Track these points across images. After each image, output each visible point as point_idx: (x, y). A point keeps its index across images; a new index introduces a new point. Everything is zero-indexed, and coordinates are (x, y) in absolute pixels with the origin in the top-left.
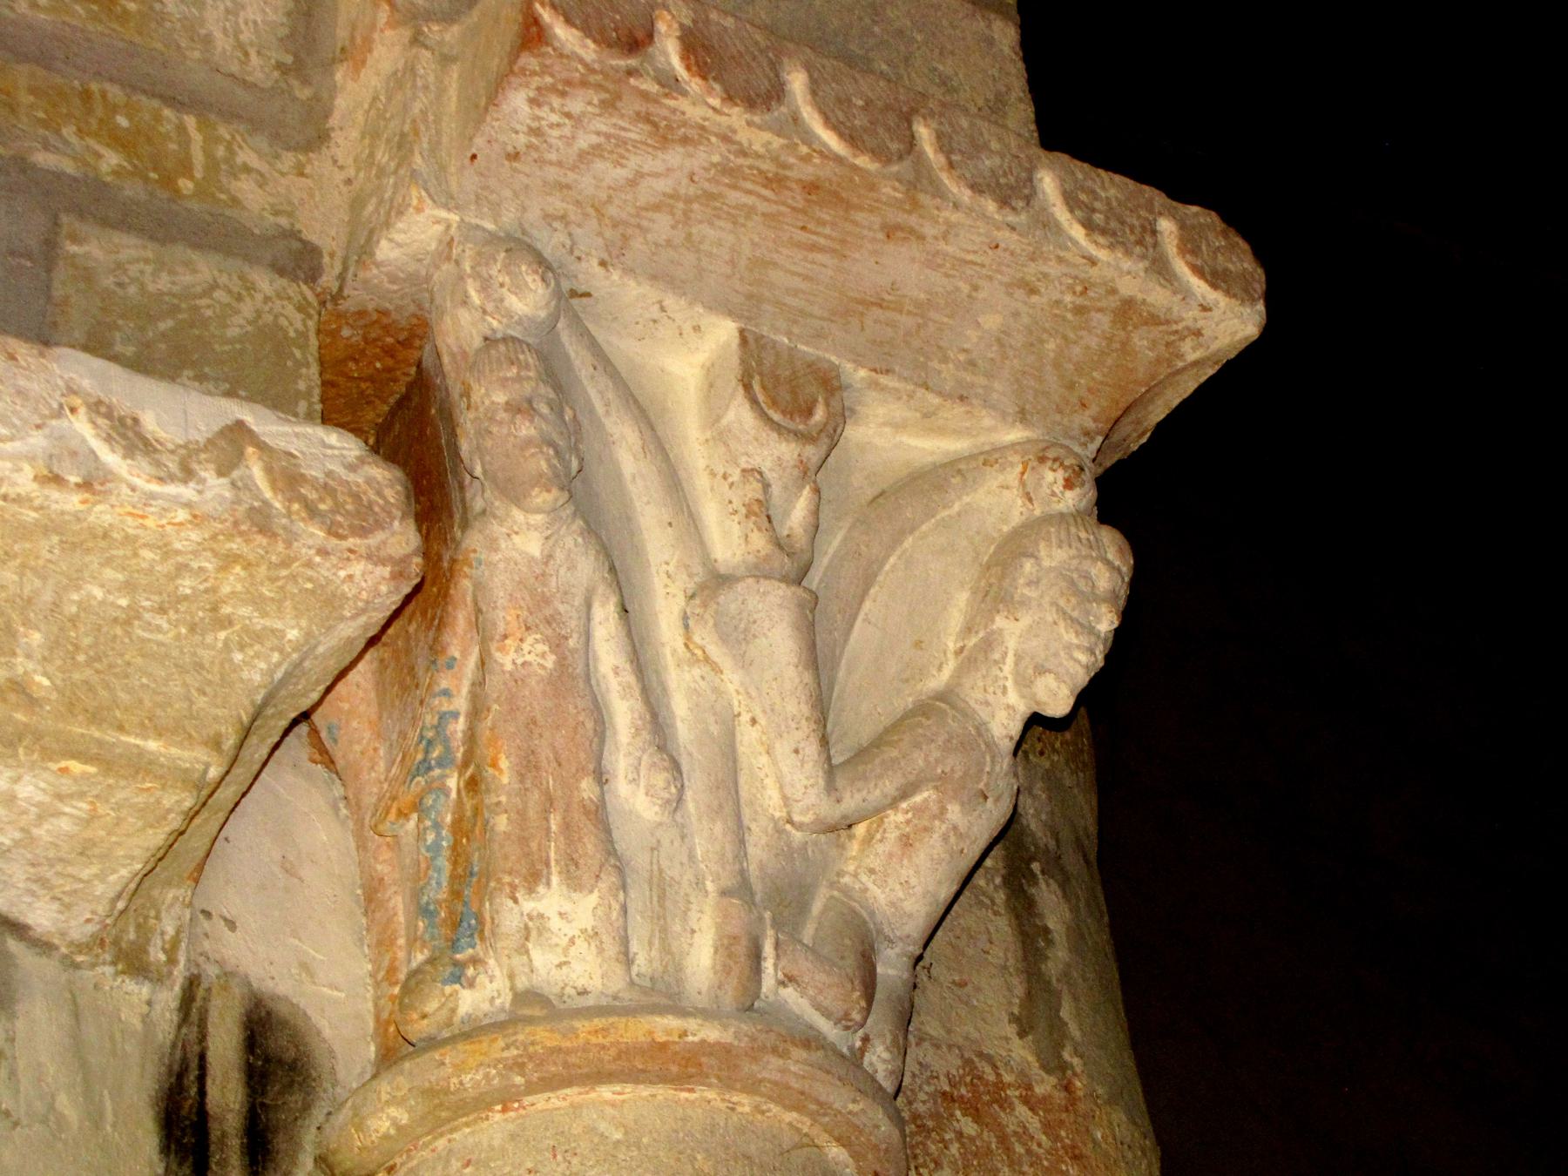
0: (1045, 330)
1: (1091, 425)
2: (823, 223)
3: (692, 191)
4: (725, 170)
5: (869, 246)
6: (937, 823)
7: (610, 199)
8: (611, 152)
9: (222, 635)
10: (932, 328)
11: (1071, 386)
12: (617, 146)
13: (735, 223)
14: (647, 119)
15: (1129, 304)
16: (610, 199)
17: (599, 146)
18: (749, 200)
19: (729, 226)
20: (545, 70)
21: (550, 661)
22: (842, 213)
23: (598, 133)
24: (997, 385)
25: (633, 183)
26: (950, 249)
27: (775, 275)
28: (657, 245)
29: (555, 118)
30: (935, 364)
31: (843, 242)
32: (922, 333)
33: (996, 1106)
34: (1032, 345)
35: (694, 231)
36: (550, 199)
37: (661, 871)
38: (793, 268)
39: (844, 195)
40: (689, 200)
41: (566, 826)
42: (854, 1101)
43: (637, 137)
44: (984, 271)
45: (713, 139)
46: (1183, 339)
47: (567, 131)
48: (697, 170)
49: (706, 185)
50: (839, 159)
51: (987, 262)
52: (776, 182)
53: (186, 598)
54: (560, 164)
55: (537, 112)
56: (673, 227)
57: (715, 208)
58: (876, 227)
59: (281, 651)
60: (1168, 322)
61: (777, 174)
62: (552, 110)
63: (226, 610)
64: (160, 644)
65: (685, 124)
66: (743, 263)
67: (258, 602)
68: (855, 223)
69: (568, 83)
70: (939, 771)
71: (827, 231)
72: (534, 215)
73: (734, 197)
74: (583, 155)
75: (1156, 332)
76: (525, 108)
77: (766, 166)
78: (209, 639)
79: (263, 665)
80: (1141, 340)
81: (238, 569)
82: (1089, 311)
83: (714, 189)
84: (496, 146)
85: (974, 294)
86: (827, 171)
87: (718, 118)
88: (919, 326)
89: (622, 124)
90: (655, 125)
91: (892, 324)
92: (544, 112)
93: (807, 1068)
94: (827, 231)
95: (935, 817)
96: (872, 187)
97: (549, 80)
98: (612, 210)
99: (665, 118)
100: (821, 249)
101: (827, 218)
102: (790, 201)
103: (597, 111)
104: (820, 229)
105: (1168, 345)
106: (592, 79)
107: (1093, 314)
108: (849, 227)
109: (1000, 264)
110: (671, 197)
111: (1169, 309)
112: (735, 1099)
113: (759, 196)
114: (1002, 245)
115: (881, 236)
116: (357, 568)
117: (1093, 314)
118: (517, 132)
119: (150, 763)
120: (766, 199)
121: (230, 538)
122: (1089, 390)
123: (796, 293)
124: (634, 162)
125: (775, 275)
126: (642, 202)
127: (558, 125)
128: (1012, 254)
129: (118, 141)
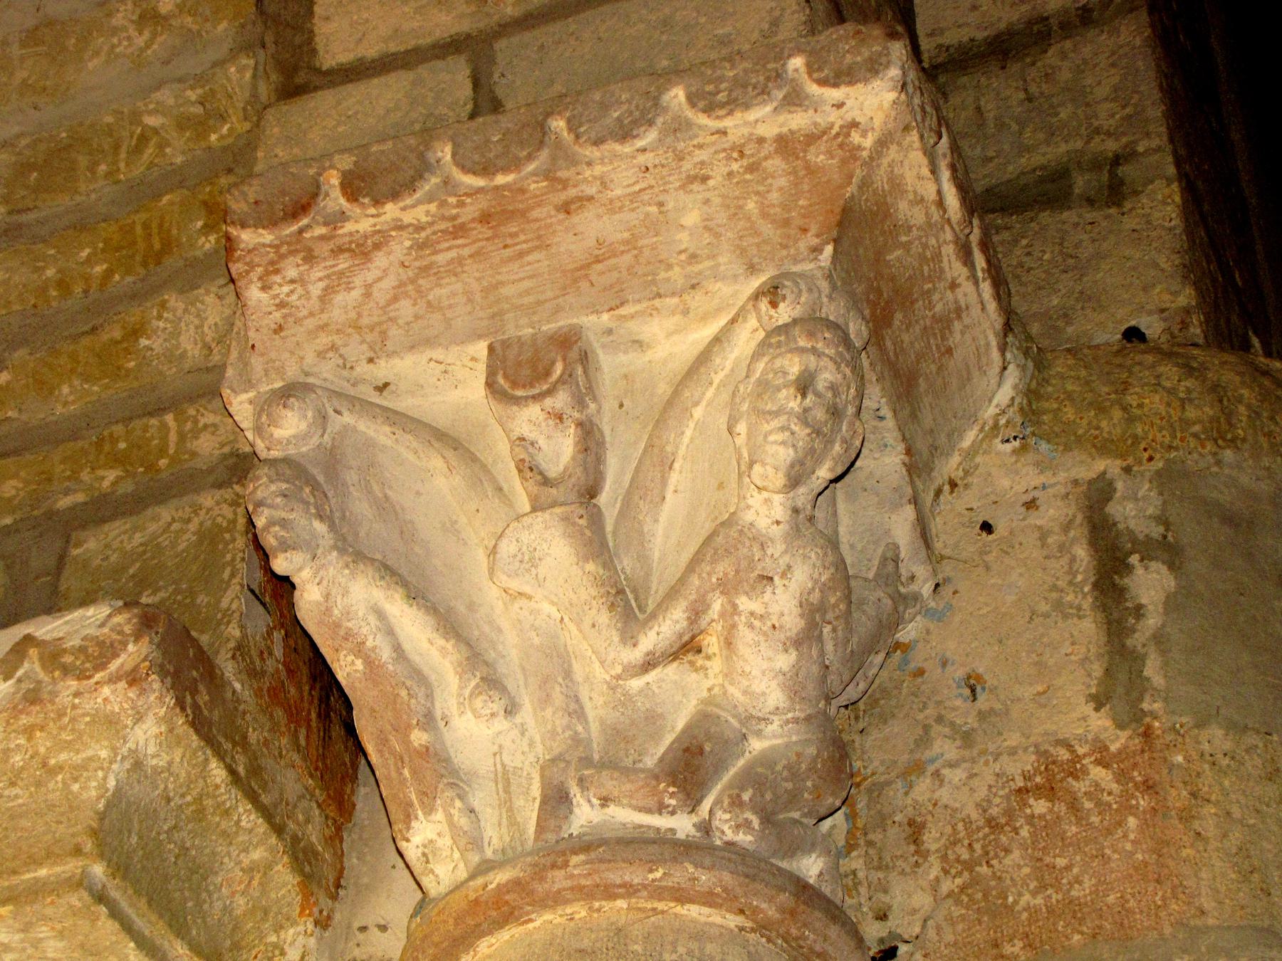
0: (737, 198)
1: (816, 241)
3: (410, 274)
6: (736, 618)
7: (359, 315)
9: (60, 777)
10: (647, 252)
11: (786, 223)
12: (339, 279)
13: (456, 275)
14: (340, 250)
16: (359, 315)
17: (325, 289)
19: (453, 279)
20: (252, 266)
21: (359, 665)
23: (320, 279)
24: (721, 260)
25: (368, 295)
27: (507, 291)
28: (408, 324)
29: (286, 289)
30: (663, 275)
31: (539, 237)
32: (641, 260)
33: (1070, 779)
34: (736, 214)
35: (430, 297)
36: (318, 341)
37: (504, 766)
38: (516, 277)
40: (413, 281)
41: (414, 772)
42: (651, 871)
43: (346, 265)
44: (656, 190)
45: (393, 233)
46: (848, 135)
47: (300, 291)
48: (402, 258)
49: (417, 264)
50: (480, 190)
51: (653, 182)
52: (459, 231)
53: (22, 768)
54: (311, 314)
55: (272, 292)
56: (414, 305)
57: (435, 274)
58: (553, 213)
59: (102, 769)
60: (824, 133)
62: (281, 285)
63: (53, 762)
64: (20, 806)
65: (366, 237)
66: (478, 297)
67: (67, 746)
68: (537, 220)
69: (272, 263)
70: (714, 580)
71: (522, 237)
72: (310, 358)
73: (441, 258)
74: (322, 299)
75: (823, 145)
76: (264, 296)
77: (443, 225)
78: (51, 785)
79: (94, 784)
80: (817, 156)
81: (38, 734)
82: (760, 164)
84: (265, 331)
86: (483, 203)
87: (382, 219)
90: (349, 250)
91: (616, 268)
92: (276, 290)
94: (522, 237)
95: (733, 614)
96: (522, 191)
97: (260, 270)
98: (365, 321)
99: (350, 242)
100: (529, 252)
103: (306, 267)
104: (517, 240)
105: (841, 146)
106: (284, 249)
107: (764, 164)
110: (399, 287)
111: (815, 124)
112: (569, 911)
113: (458, 247)
114: (649, 165)
115: (562, 216)
116: (106, 691)
117: (764, 164)
119: (44, 884)
120: (465, 245)
121: (16, 717)
122: (804, 216)
123: (527, 292)
124: (358, 281)
125: (507, 291)
126: (382, 302)
127: (292, 292)
128: (663, 166)
129: (118, 460)
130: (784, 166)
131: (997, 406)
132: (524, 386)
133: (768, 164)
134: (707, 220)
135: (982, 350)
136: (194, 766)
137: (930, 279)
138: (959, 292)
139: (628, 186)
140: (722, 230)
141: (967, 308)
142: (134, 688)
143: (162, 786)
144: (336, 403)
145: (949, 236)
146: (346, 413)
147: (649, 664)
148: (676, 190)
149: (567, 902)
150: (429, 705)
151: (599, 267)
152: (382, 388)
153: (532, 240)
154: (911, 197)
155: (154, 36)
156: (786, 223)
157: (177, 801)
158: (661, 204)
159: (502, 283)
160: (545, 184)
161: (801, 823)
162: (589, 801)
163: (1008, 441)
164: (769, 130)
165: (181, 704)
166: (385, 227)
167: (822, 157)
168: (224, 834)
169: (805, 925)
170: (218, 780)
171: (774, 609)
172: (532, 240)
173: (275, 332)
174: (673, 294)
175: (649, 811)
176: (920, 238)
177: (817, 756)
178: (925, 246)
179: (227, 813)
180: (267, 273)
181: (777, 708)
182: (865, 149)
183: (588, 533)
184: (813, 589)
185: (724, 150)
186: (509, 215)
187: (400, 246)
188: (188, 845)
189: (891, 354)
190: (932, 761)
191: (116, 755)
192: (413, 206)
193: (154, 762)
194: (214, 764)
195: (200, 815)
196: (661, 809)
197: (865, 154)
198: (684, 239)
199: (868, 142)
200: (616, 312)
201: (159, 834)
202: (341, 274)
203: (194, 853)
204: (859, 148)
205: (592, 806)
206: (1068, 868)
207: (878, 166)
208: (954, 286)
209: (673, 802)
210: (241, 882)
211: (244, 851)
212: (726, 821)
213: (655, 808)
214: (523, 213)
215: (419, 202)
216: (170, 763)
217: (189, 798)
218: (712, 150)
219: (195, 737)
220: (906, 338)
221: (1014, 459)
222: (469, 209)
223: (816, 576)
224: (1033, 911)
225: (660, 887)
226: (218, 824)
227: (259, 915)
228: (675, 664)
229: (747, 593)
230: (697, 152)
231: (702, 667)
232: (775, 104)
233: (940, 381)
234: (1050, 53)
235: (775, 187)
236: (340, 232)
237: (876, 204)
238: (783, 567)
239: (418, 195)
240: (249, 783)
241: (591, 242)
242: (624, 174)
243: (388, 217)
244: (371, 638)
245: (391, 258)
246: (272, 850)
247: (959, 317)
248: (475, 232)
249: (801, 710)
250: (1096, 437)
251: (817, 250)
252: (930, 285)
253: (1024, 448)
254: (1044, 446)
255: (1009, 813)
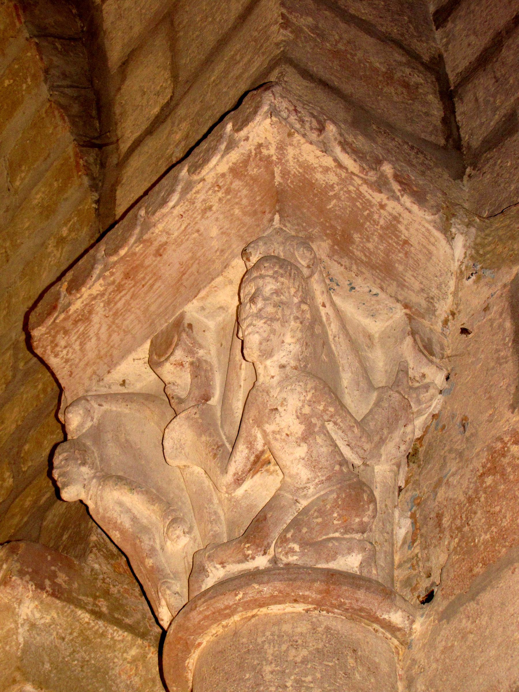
0: (229, 211)
2: (144, 278)
3: (111, 319)
4: (108, 303)
5: (161, 265)
7: (99, 351)
8: (85, 340)
10: (202, 259)
12: (83, 336)
14: (76, 322)
15: (232, 170)
16: (99, 351)
18: (123, 301)
19: (129, 313)
22: (142, 269)
23: (76, 341)
25: (98, 339)
26: (176, 234)
27: (153, 308)
29: (65, 352)
31: (155, 274)
39: (134, 265)
40: (113, 322)
42: (236, 595)
44: (192, 224)
45: (93, 302)
46: (261, 152)
48: (104, 313)
49: (111, 313)
51: (188, 221)
52: (119, 288)
54: (80, 360)
56: (119, 334)
58: (154, 259)
60: (249, 156)
61: (116, 286)
62: (62, 351)
65: (83, 310)
68: (149, 266)
69: (52, 342)
71: (148, 278)
73: (120, 305)
74: (81, 350)
77: (111, 288)
80: (253, 171)
82: (230, 188)
83: (114, 310)
84: (65, 377)
85: (200, 233)
88: (198, 264)
89: (75, 331)
90: (80, 320)
91: (192, 274)
93: (205, 604)
94: (148, 278)
96: (135, 254)
97: (49, 347)
98: (103, 352)
99: (78, 315)
101: (142, 276)
102: (130, 286)
106: (53, 333)
108: (149, 269)
109: (191, 217)
110: (109, 328)
111: (243, 154)
113: (123, 296)
114: (182, 213)
115: (159, 258)
118: (64, 368)
120: (126, 294)
124: (92, 334)
126: (106, 340)
127: (68, 352)
128: (188, 211)
130: (241, 183)
131: (458, 260)
132: (163, 356)
133: (234, 186)
134: (221, 229)
135: (426, 234)
136: (67, 616)
137: (364, 209)
138: (389, 208)
139: (178, 229)
140: (229, 231)
141: (400, 215)
142: (8, 587)
143: (55, 633)
144: (99, 401)
145: (359, 181)
146: (104, 404)
147: (239, 481)
148: (201, 220)
149: (208, 627)
150: (152, 543)
151: (186, 276)
152: (123, 383)
153: (152, 277)
154: (320, 170)
155: (62, 249)
156: (255, 213)
157: (68, 638)
158: (198, 231)
159: (149, 306)
160: (141, 245)
161: (344, 539)
162: (215, 567)
163: (469, 278)
164: (223, 168)
165: (41, 587)
166: (88, 301)
167: (255, 170)
168: (107, 646)
169: (339, 596)
170: (87, 620)
171: (283, 424)
172: (152, 277)
173: (70, 376)
174: (218, 275)
175: (240, 562)
176: (342, 189)
177: (338, 497)
178: (349, 192)
179: (103, 635)
180: (53, 348)
181: (308, 479)
182: (272, 156)
183: (200, 421)
184: (303, 406)
185: (210, 189)
186: (136, 269)
187: (99, 307)
188: (87, 658)
189: (363, 258)
190: (445, 476)
191: (17, 624)
192: (93, 285)
193: (42, 621)
194: (79, 612)
195: (87, 641)
196: (246, 558)
197: (274, 158)
198: (215, 244)
199: (272, 151)
200: (197, 297)
201: (64, 658)
202: (83, 333)
203: (93, 662)
204: (269, 156)
205: (217, 569)
206: (500, 511)
207: (287, 161)
208: (382, 206)
209: (250, 552)
210: (131, 670)
211: (124, 652)
212: (281, 552)
213: (244, 559)
214: (141, 265)
215: (95, 281)
216: (53, 618)
217: (75, 634)
218: (204, 192)
219: (58, 601)
220: (370, 245)
221: (476, 287)
222: (118, 274)
223: (302, 398)
224: (485, 543)
225: (246, 602)
226: (101, 643)
227: (150, 684)
228: (259, 475)
229: (267, 423)
230: (198, 196)
231: (274, 471)
232: (222, 153)
233: (411, 261)
234: (503, 50)
235: (243, 196)
236: (70, 313)
237: (300, 181)
238: (281, 400)
239: (93, 279)
240: (113, 617)
241: (177, 266)
242: (173, 223)
243: (85, 296)
244: (118, 518)
245: (99, 314)
246: (141, 647)
247: (399, 222)
248: (127, 285)
249: (322, 475)
250: (511, 256)
251: (272, 220)
252: (368, 212)
253: (479, 279)
254: (488, 272)
255: (476, 491)
